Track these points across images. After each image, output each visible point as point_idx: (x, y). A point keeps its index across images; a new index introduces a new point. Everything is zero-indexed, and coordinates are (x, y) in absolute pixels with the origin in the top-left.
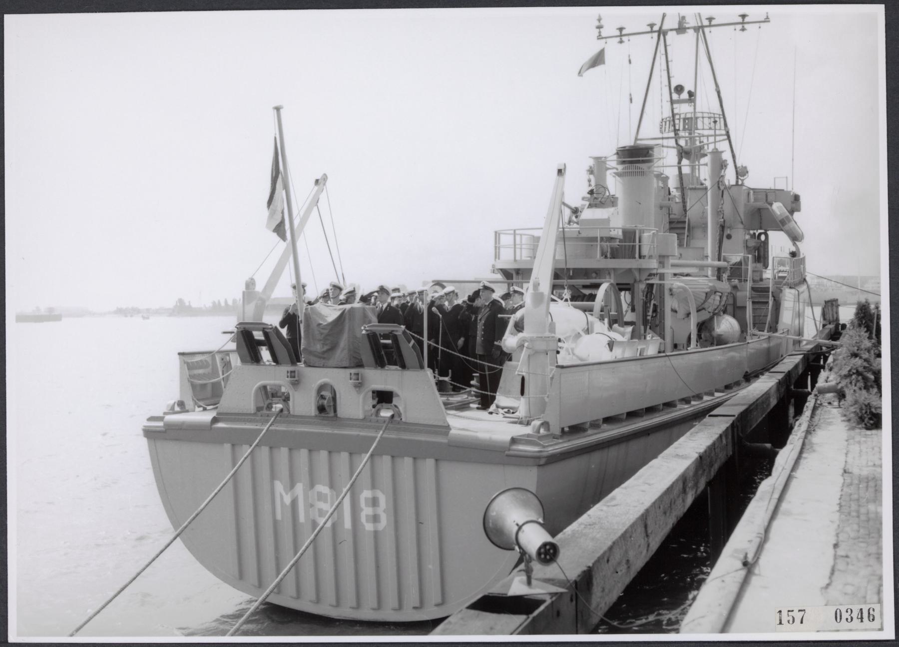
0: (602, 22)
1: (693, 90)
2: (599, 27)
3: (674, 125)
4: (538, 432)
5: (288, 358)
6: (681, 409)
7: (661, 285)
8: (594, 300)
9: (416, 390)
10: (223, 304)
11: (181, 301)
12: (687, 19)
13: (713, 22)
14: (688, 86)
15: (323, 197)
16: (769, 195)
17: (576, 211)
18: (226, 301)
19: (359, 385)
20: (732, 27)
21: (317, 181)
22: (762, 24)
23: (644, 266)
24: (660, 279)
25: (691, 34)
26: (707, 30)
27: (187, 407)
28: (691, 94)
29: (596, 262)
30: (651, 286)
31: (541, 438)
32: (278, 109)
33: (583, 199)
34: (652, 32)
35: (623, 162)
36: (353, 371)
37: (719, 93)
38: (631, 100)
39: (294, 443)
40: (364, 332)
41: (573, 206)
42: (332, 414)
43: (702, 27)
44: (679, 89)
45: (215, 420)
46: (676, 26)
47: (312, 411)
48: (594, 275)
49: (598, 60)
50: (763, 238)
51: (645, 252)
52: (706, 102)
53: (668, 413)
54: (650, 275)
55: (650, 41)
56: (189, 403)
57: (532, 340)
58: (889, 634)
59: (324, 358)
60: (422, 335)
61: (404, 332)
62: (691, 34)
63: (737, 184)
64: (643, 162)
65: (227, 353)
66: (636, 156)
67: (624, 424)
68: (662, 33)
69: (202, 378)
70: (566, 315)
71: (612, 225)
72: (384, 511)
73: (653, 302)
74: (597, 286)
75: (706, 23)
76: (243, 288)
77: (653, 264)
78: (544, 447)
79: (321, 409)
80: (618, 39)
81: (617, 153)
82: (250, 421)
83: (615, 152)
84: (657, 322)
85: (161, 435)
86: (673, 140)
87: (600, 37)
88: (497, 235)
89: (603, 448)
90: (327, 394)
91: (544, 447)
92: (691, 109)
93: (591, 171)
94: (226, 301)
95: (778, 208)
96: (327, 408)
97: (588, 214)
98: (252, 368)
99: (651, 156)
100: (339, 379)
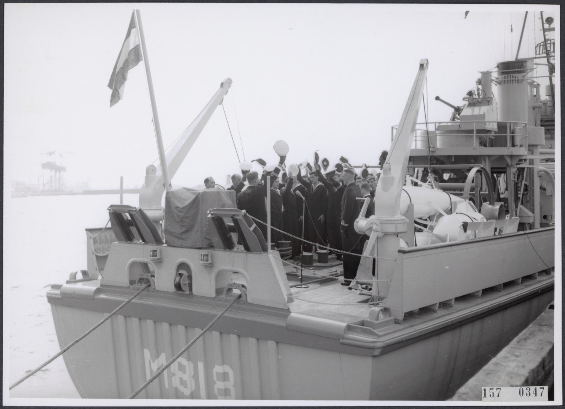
3: (546, 48)
4: (377, 319)
5: (153, 238)
6: (540, 282)
7: (530, 168)
8: (464, 182)
9: (263, 274)
17: (458, 110)
21: (222, 84)
23: (514, 154)
24: (530, 164)
29: (474, 148)
30: (521, 170)
33: (464, 99)
35: (503, 73)
36: (204, 252)
38: (512, 30)
39: (158, 316)
40: (210, 216)
41: (456, 105)
42: (187, 292)
45: (98, 291)
47: (172, 289)
48: (473, 161)
51: (518, 141)
53: (527, 286)
54: (521, 160)
57: (382, 222)
59: (182, 239)
60: (266, 221)
61: (245, 216)
64: (519, 72)
67: (480, 301)
70: (428, 197)
71: (487, 120)
72: (233, 386)
73: (524, 182)
74: (469, 170)
77: (522, 151)
78: (379, 336)
79: (178, 287)
81: (498, 67)
83: (496, 65)
84: (528, 199)
86: (546, 59)
88: (392, 128)
89: (454, 328)
91: (379, 336)
93: (479, 82)
96: (183, 286)
97: (467, 112)
98: (125, 247)
100: (193, 258)
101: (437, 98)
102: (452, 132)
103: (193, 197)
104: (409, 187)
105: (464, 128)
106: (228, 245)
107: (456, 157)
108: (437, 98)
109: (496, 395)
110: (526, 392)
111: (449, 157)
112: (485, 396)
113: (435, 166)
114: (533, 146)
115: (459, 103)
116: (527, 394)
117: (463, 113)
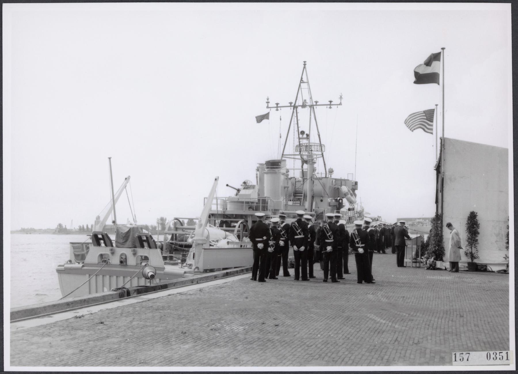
0: (269, 100)
1: (308, 133)
2: (268, 103)
10: (85, 227)
11: (60, 225)
12: (307, 101)
13: (318, 104)
14: (307, 132)
15: (128, 185)
16: (342, 182)
17: (238, 190)
18: (87, 226)
19: (135, 254)
20: (326, 106)
21: (126, 179)
22: (339, 106)
25: (307, 109)
26: (315, 107)
27: (73, 262)
28: (308, 135)
31: (195, 272)
32: (110, 158)
33: (241, 185)
34: (291, 106)
37: (319, 135)
41: (237, 188)
43: (313, 105)
44: (303, 133)
45: (83, 266)
46: (301, 104)
47: (118, 262)
49: (266, 116)
50: (340, 201)
52: (314, 139)
55: (290, 110)
56: (73, 260)
57: (197, 240)
58: (512, 367)
62: (307, 109)
63: (326, 177)
64: (277, 168)
65: (88, 244)
66: (274, 165)
68: (295, 107)
69: (79, 252)
70: (216, 232)
75: (314, 104)
76: (95, 219)
79: (121, 262)
80: (276, 109)
82: (97, 267)
85: (62, 271)
87: (268, 107)
90: (124, 257)
92: (308, 142)
94: (87, 226)
95: (344, 189)
96: (123, 262)
97: (243, 192)
98: (97, 248)
99: (280, 165)
100: (128, 252)
101: (227, 185)
102: (234, 202)
103: (128, 230)
104: (208, 227)
105: (240, 200)
106: (142, 246)
107: (236, 215)
108: (227, 185)
109: (465, 359)
110: (492, 356)
111: (233, 215)
112: (456, 361)
113: (225, 221)
114: (277, 210)
115: (238, 186)
116: (500, 359)
117: (241, 193)
